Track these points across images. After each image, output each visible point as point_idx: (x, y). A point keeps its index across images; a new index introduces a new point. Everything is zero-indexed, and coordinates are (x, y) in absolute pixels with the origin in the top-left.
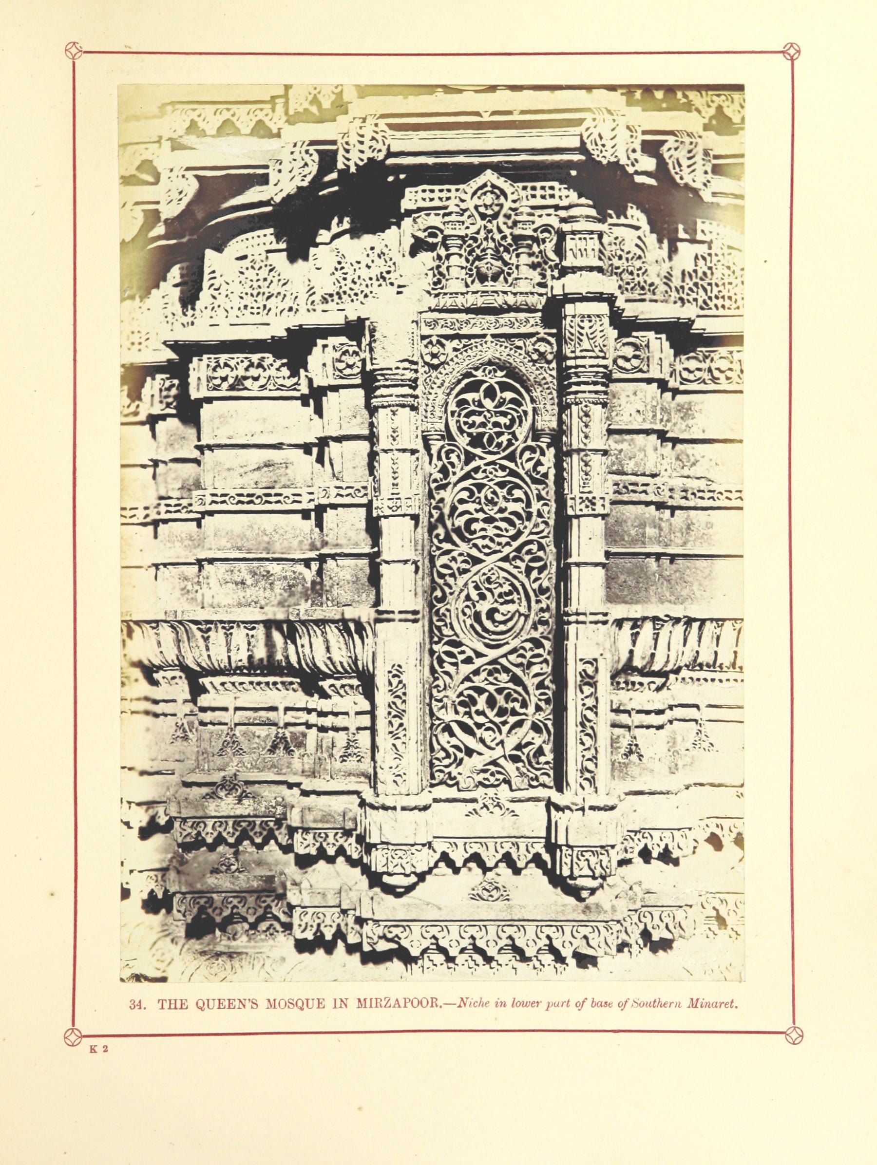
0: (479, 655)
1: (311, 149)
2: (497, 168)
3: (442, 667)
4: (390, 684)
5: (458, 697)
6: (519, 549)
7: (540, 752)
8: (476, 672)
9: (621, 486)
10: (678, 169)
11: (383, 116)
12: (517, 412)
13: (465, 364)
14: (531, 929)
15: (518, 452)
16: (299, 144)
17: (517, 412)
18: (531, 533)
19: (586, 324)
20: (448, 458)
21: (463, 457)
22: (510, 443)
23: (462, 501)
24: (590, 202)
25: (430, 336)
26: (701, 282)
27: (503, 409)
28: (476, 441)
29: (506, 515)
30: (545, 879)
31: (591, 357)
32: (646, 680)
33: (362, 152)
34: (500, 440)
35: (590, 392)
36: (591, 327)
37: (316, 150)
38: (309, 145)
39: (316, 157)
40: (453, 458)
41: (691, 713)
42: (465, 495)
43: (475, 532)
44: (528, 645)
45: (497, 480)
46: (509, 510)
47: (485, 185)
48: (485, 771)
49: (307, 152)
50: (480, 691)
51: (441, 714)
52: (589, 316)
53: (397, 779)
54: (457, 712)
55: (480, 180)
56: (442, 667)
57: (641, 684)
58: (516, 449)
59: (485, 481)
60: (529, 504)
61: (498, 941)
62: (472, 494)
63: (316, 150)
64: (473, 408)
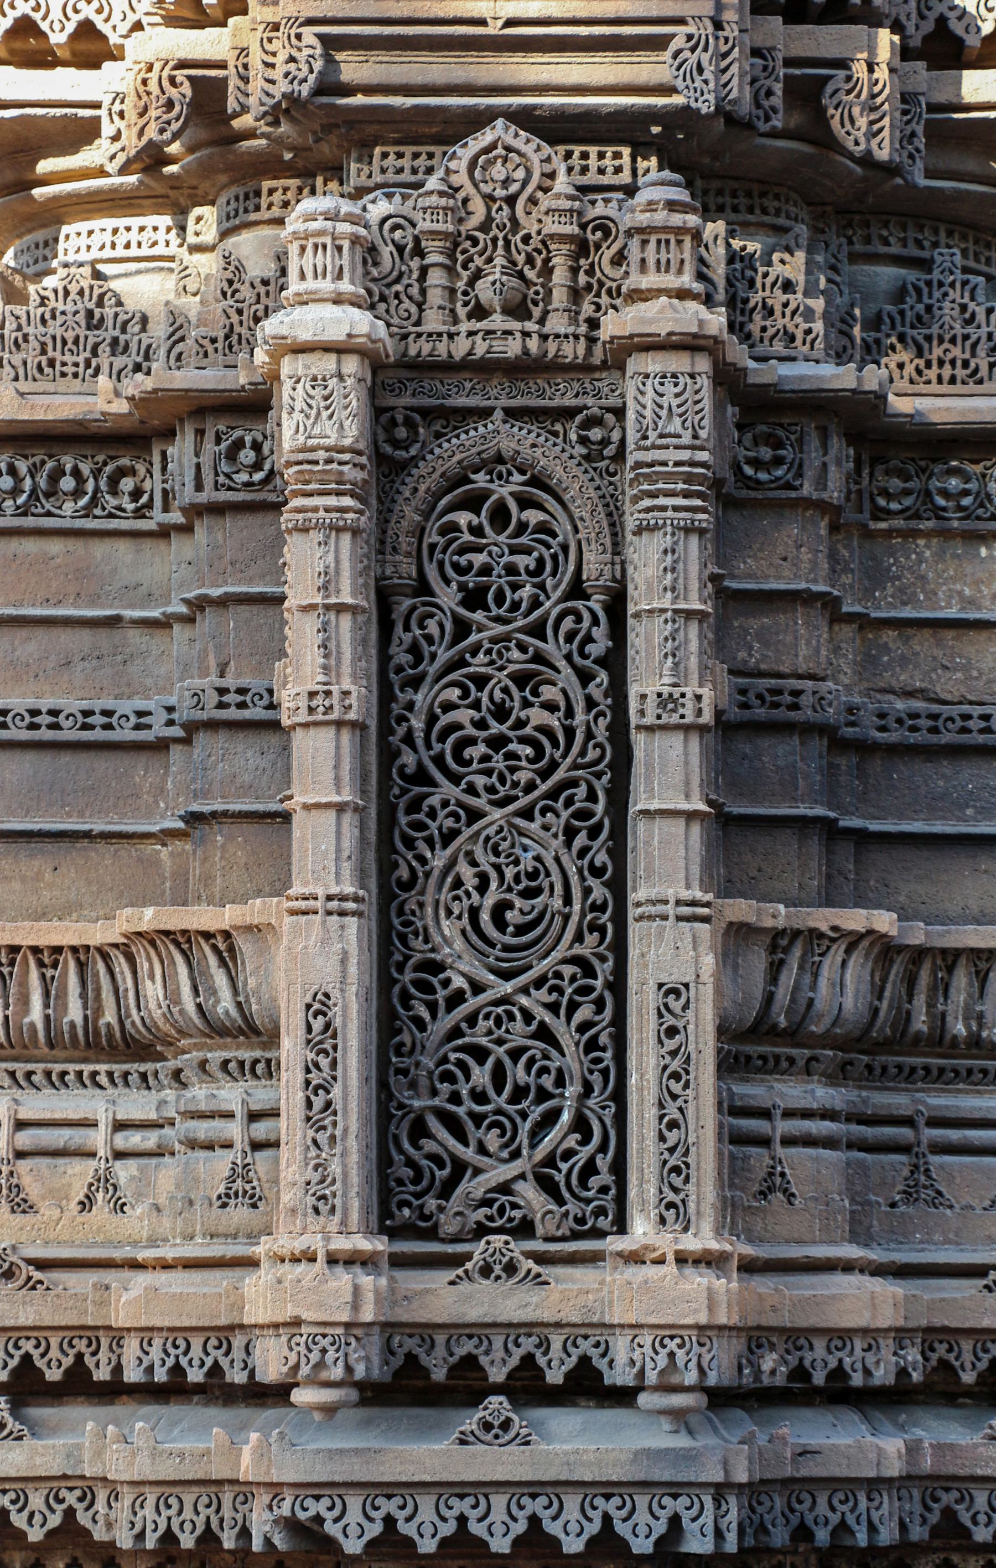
0: (477, 988)
1: (180, 75)
2: (524, 119)
3: (408, 1008)
4: (309, 1029)
5: (438, 1065)
6: (553, 794)
7: (590, 1169)
8: (472, 1020)
9: (751, 695)
10: (848, 126)
11: (310, 22)
12: (549, 547)
13: (455, 459)
14: (572, 1503)
15: (550, 622)
16: (157, 67)
17: (549, 547)
18: (575, 766)
19: (669, 389)
20: (422, 627)
21: (448, 626)
22: (535, 604)
23: (448, 707)
24: (677, 177)
25: (393, 409)
26: (910, 332)
27: (524, 540)
28: (474, 599)
29: (528, 730)
30: (72, 70)
31: (676, 447)
32: (801, 1054)
33: (272, 82)
34: (516, 596)
35: (676, 509)
36: (677, 395)
37: (189, 78)
38: (176, 68)
39: (187, 89)
40: (432, 627)
41: (905, 1133)
42: (454, 694)
43: (469, 763)
44: (568, 970)
45: (512, 668)
46: (533, 723)
47: (493, 146)
48: (487, 1203)
49: (172, 80)
50: (480, 1054)
51: (405, 1096)
52: (674, 376)
53: (321, 1205)
54: (434, 1093)
55: (487, 137)
56: (408, 1008)
57: (791, 1060)
58: (548, 613)
59: (489, 670)
60: (570, 713)
61: (512, 1524)
62: (466, 694)
63: (189, 78)
64: (467, 537)
